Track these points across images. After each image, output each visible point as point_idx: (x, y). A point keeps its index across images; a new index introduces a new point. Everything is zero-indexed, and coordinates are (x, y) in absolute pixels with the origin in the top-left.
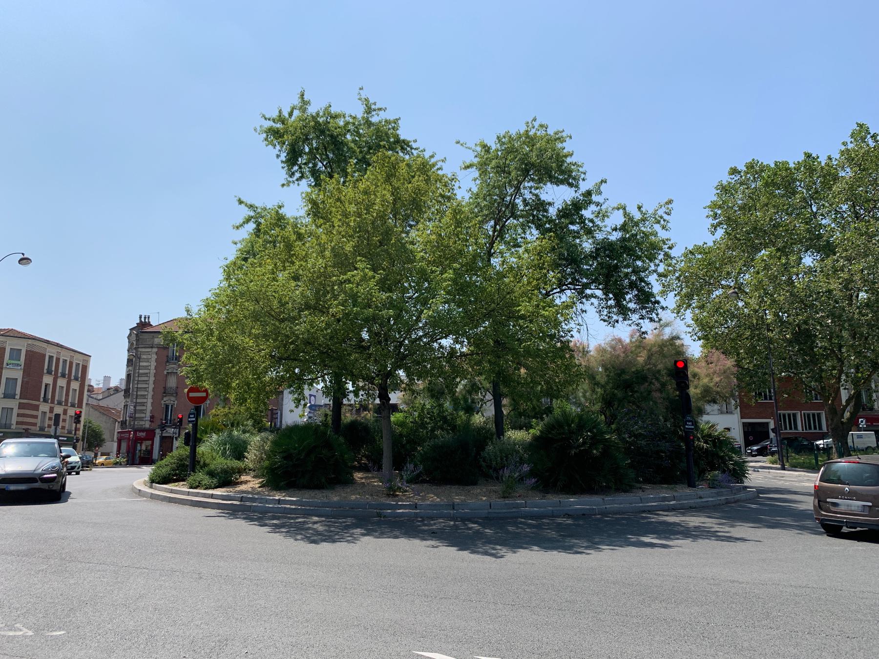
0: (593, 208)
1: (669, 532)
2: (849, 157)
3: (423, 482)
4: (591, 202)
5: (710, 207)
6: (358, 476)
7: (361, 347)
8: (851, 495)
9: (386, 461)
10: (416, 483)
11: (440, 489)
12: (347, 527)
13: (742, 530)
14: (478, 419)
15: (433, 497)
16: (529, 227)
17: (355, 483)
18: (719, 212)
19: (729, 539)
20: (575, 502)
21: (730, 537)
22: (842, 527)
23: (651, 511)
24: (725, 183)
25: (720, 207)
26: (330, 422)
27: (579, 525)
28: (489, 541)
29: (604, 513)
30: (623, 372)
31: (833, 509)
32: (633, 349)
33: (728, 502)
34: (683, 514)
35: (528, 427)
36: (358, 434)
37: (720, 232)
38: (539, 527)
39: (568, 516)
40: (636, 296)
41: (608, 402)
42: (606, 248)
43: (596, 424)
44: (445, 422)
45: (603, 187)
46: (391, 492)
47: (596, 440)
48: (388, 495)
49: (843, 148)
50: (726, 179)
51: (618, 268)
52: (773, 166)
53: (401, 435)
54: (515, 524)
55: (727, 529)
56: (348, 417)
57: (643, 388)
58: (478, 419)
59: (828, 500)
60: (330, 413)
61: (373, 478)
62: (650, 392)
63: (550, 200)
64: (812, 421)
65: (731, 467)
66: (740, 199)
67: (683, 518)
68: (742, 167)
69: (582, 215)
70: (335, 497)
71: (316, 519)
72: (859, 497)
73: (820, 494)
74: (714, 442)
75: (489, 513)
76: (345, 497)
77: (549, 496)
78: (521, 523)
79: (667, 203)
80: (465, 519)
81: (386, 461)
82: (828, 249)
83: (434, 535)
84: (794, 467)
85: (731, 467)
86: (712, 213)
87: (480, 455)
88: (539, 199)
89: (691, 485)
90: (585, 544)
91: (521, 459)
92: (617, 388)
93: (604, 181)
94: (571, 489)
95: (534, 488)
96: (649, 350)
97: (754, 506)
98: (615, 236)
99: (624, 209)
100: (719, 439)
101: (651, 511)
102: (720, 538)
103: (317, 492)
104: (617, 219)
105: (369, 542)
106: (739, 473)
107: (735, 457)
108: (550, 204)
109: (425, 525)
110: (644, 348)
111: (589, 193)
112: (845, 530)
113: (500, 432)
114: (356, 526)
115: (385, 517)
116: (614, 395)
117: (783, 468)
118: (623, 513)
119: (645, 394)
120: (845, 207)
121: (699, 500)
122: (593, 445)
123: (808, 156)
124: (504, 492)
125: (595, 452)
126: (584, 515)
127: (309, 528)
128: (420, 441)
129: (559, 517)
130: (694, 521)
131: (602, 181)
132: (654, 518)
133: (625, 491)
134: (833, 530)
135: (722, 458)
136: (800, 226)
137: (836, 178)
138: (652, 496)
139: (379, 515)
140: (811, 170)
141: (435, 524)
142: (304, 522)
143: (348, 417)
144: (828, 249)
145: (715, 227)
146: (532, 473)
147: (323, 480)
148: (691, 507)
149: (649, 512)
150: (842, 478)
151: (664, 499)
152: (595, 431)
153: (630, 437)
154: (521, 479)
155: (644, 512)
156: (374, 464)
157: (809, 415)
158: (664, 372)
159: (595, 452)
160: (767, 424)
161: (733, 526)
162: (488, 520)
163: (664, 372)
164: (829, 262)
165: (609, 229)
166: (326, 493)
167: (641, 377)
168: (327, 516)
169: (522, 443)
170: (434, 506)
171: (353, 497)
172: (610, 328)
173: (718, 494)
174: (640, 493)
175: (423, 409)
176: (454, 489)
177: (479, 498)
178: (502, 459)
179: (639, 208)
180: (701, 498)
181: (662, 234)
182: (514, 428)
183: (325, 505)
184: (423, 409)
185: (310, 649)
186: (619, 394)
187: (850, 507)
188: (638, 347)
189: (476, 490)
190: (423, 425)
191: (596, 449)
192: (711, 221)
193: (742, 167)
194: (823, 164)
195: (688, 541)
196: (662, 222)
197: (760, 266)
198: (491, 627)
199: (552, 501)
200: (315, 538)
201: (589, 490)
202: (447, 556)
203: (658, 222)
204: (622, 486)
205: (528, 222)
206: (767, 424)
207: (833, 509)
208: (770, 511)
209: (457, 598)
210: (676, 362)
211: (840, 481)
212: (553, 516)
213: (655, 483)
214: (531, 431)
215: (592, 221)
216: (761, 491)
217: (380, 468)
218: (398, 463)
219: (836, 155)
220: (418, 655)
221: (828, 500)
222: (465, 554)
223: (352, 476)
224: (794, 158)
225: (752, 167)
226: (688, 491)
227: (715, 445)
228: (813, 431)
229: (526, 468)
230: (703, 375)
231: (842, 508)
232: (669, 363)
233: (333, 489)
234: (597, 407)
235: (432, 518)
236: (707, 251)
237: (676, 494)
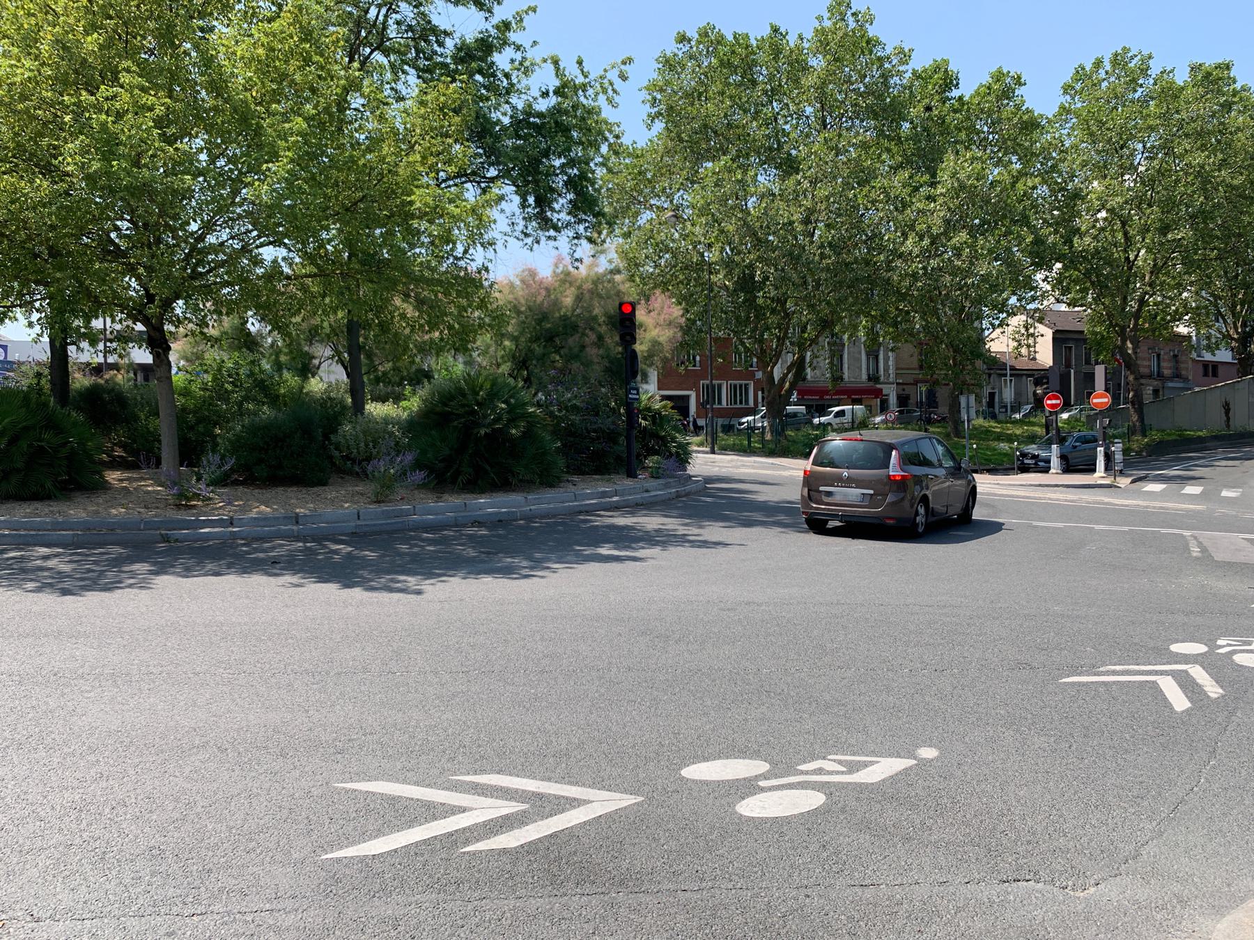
0: (509, 52)
1: (627, 538)
2: (823, 42)
3: (236, 483)
4: (505, 43)
5: (647, 88)
6: (113, 476)
7: (111, 252)
8: (849, 482)
9: (168, 451)
10: (225, 485)
11: (268, 494)
12: (118, 562)
13: (714, 531)
14: (316, 385)
15: (261, 508)
16: (404, 72)
17: (110, 489)
18: (659, 97)
19: (705, 544)
20: (487, 504)
21: (705, 542)
22: (827, 521)
23: (589, 511)
24: (669, 54)
25: (661, 90)
26: (48, 386)
27: (499, 536)
28: (379, 571)
29: (529, 518)
30: (543, 317)
31: (826, 499)
32: (557, 284)
33: (678, 495)
34: (633, 514)
35: (398, 398)
36: (104, 405)
37: (659, 126)
38: (444, 541)
39: (478, 523)
40: (571, 201)
41: (521, 362)
42: (524, 123)
43: (513, 392)
44: (264, 388)
45: (527, 20)
46: (183, 500)
47: (516, 413)
48: (179, 506)
49: (817, 25)
50: (672, 48)
51: (545, 154)
52: (730, 38)
53: (184, 409)
54: (406, 541)
55: (696, 531)
56: (80, 381)
57: (572, 341)
58: (316, 385)
59: (821, 488)
60: (46, 372)
61: (142, 479)
62: (583, 347)
63: (449, 28)
64: (738, 393)
65: (674, 450)
66: (688, 80)
67: (635, 520)
68: (693, 34)
69: (493, 63)
70: (78, 511)
71: (44, 551)
72: (859, 483)
73: (810, 481)
74: (653, 417)
75: (357, 526)
76: (97, 512)
77: (446, 496)
78: (413, 538)
79: (624, 63)
80: (321, 538)
81: (168, 451)
82: (789, 166)
83: (270, 566)
84: (725, 449)
85: (674, 450)
86: (650, 98)
87: (329, 439)
88: (429, 22)
89: (631, 474)
90: (525, 563)
91: (397, 444)
92: (536, 339)
93: (534, 10)
94: (476, 485)
95: (423, 486)
96: (579, 288)
97: (708, 499)
98: (542, 106)
99: (556, 62)
100: (660, 414)
101: (589, 511)
102: (694, 544)
103: (38, 505)
104: (545, 78)
105: (167, 583)
106: (682, 457)
107: (679, 438)
108: (446, 34)
109: (256, 550)
110: (571, 284)
111: (506, 26)
112: (833, 524)
113: (359, 406)
114: (132, 560)
115: (177, 541)
116: (530, 350)
117: (713, 452)
118: (554, 516)
119: (576, 350)
120: (809, 110)
121: (647, 495)
122: (513, 421)
123: (776, 30)
124: (377, 494)
125: (514, 431)
126: (499, 522)
127: (41, 569)
128: (220, 420)
129: (464, 526)
130: (651, 522)
131: (529, 8)
132: (598, 522)
133: (551, 486)
134: (817, 526)
135: (663, 438)
136: (756, 130)
137: (806, 68)
138: (589, 490)
139: (166, 539)
140: (776, 51)
141: (273, 548)
142: (22, 557)
143: (80, 381)
144: (789, 166)
145: (653, 118)
146: (418, 465)
147: (49, 484)
148: (637, 505)
149: (587, 512)
150: (836, 462)
151: (604, 495)
152: (512, 401)
153: (560, 411)
154: (403, 474)
155: (580, 512)
156: (141, 455)
157: (735, 386)
158: (602, 319)
159: (514, 431)
160: (688, 397)
161: (701, 527)
162: (358, 537)
163: (602, 319)
164: (790, 182)
165: (535, 91)
166: (55, 506)
167: (569, 326)
168: (64, 546)
169: (387, 420)
170: (263, 520)
171: (114, 511)
172: (526, 252)
173: (667, 486)
174: (571, 488)
175: (219, 370)
176: (292, 492)
177: (338, 505)
178: (367, 445)
179: (580, 63)
180: (647, 491)
181: (607, 113)
182: (376, 399)
183: (57, 526)
184: (219, 370)
185: (121, 810)
186: (538, 349)
187: (849, 496)
188: (563, 282)
189: (330, 493)
190: (224, 396)
191: (516, 427)
192: (648, 108)
193: (693, 34)
194: (792, 45)
195: (656, 551)
196: (610, 92)
197: (710, 182)
198: (449, 715)
199: (451, 505)
200: (63, 586)
201: (503, 484)
202: (323, 598)
203: (605, 91)
204: (548, 480)
205: (404, 62)
206: (688, 397)
207: (826, 499)
208: (733, 506)
209: (365, 670)
210: (621, 305)
211: (832, 464)
212: (456, 524)
213: (583, 473)
214: (404, 403)
215: (507, 76)
216: (709, 480)
217: (158, 464)
218: (190, 454)
219: (809, 34)
220: (347, 791)
221: (821, 488)
222: (357, 593)
223: (103, 477)
224: (757, 32)
225: (706, 35)
226: (629, 482)
227: (654, 423)
228: (738, 406)
229: (409, 458)
230: (651, 326)
231: (837, 499)
232: (612, 307)
233: (69, 499)
234: (505, 368)
235: (262, 539)
236: (639, 152)
237: (618, 488)
